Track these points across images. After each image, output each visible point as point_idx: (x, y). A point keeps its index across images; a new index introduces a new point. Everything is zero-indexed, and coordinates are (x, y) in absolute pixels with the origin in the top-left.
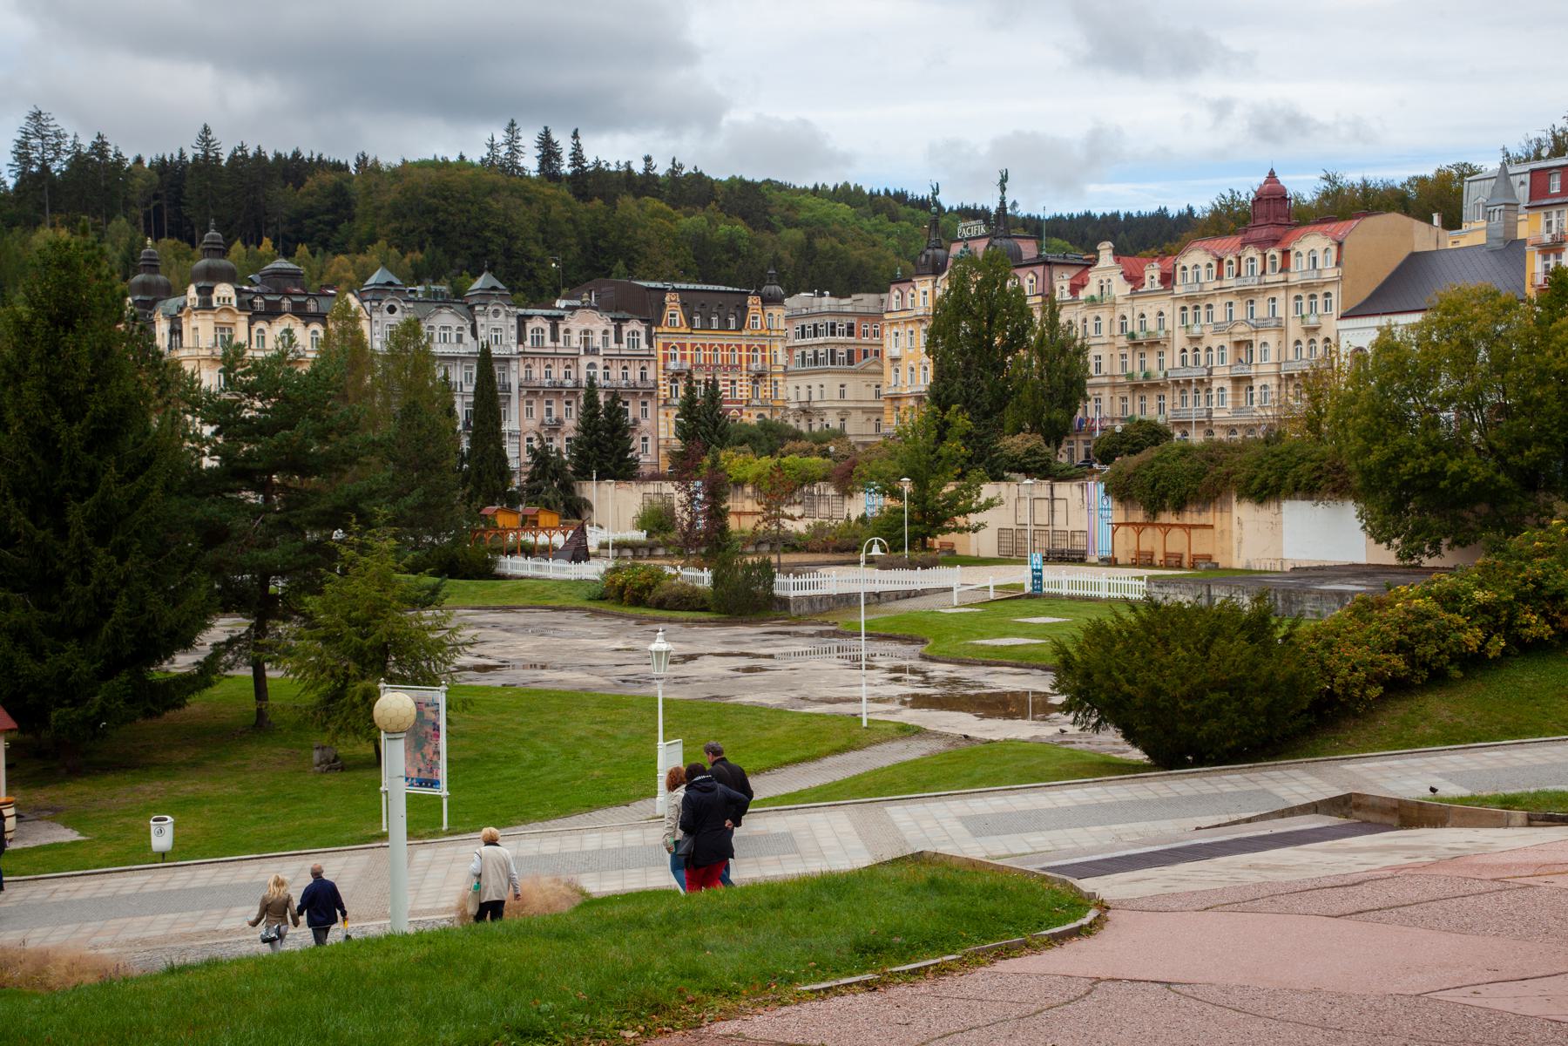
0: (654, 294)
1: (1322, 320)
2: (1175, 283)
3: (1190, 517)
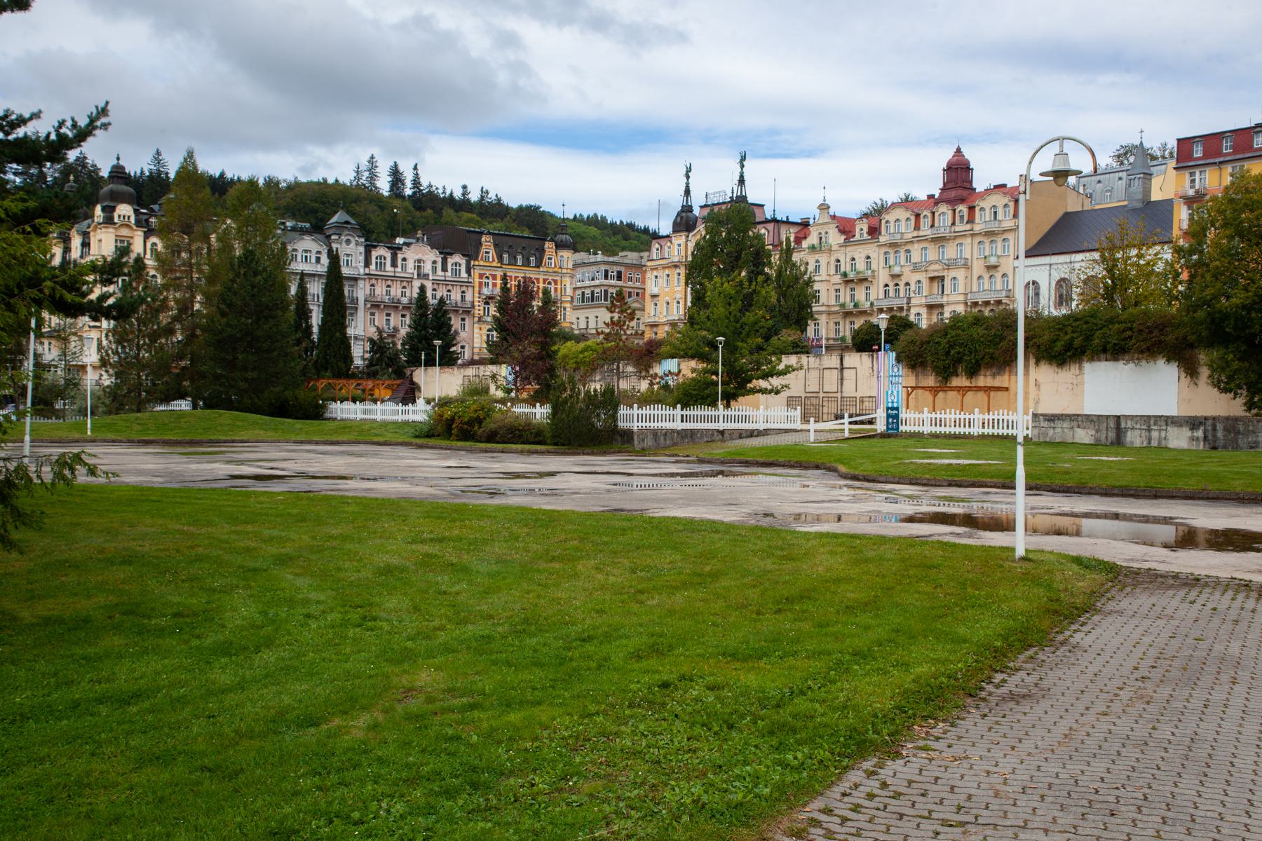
0: (473, 236)
1: (1001, 260)
2: (880, 234)
3: (983, 380)
